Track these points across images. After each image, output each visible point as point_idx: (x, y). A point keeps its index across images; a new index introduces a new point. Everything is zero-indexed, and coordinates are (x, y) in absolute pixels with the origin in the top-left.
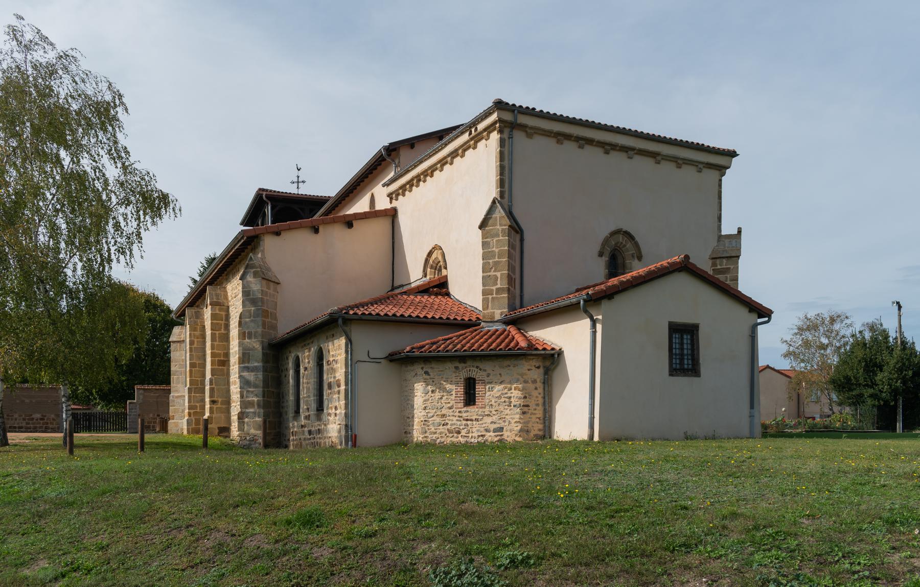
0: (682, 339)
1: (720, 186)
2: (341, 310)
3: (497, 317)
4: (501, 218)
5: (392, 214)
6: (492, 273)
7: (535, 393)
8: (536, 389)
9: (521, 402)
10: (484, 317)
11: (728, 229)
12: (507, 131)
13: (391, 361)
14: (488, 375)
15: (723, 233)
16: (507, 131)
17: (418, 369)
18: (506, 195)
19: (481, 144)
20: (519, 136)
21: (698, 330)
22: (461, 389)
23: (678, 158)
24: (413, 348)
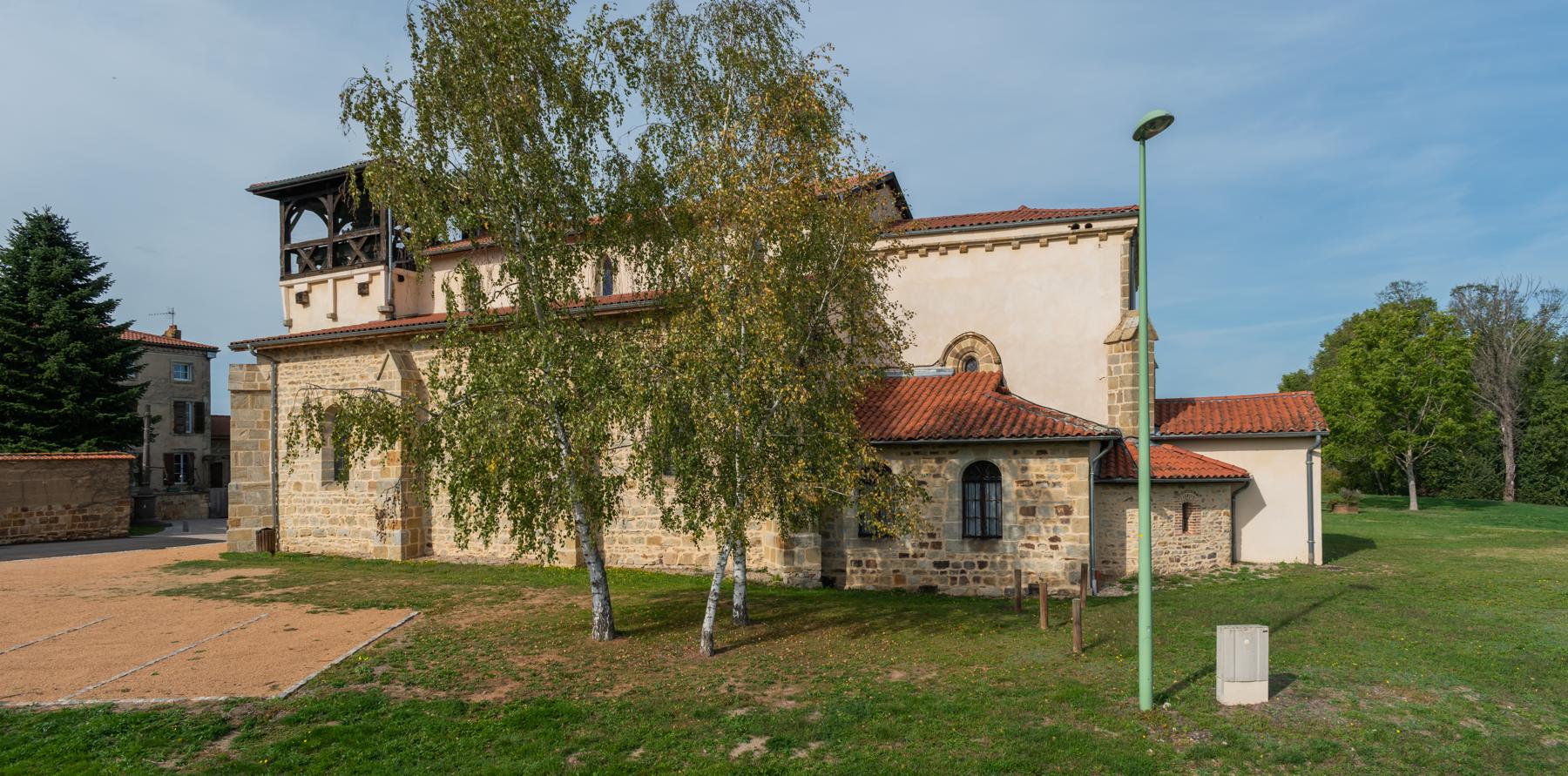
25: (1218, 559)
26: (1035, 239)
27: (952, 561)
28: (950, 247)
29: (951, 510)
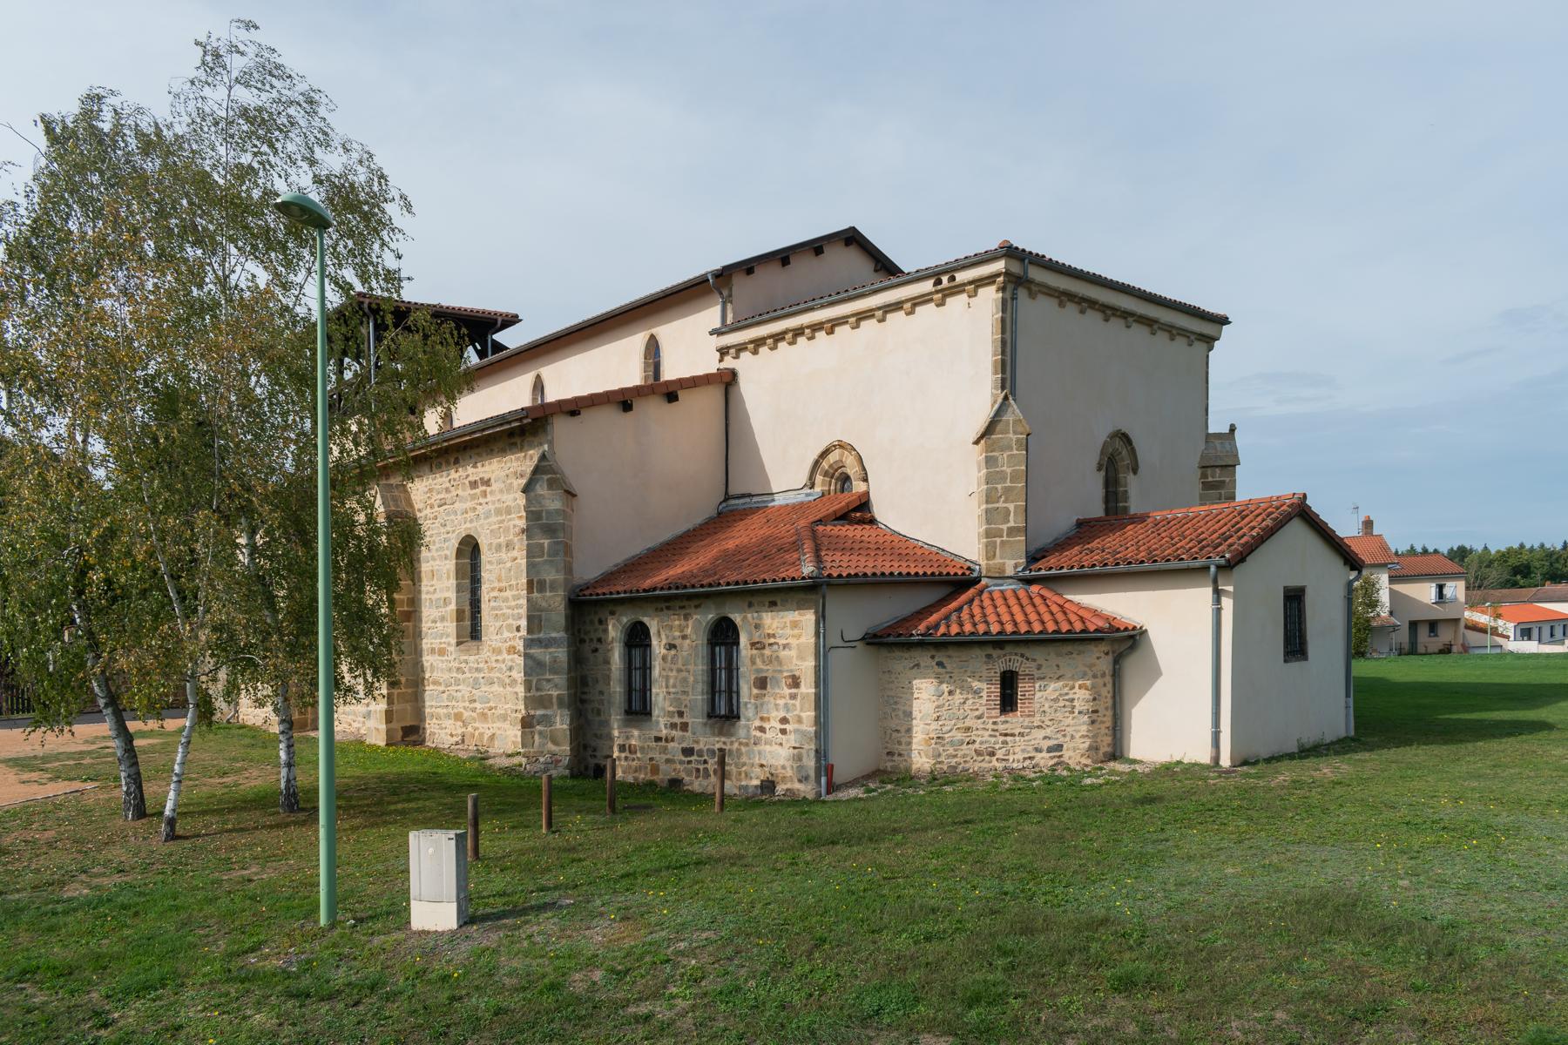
3: (1010, 572)
5: (728, 381)
6: (1001, 505)
9: (1089, 706)
10: (988, 570)
12: (1010, 287)
15: (1211, 431)
17: (924, 658)
19: (957, 302)
20: (1022, 293)
25: (1067, 755)
26: (896, 306)
27: (697, 747)
28: (778, 338)
29: (696, 681)
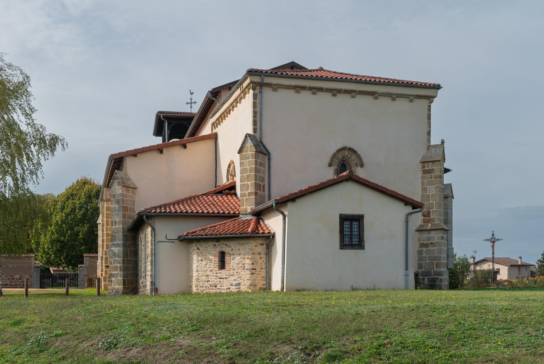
0: (351, 225)
1: (429, 110)
2: (146, 210)
3: (249, 211)
4: (251, 146)
5: (214, 137)
6: (246, 183)
7: (260, 261)
8: (261, 258)
11: (435, 140)
12: (258, 88)
13: (181, 241)
14: (232, 250)
15: (432, 144)
16: (258, 88)
17: (194, 246)
18: (258, 131)
21: (363, 219)
22: (217, 259)
23: (392, 94)
24: (188, 233)
